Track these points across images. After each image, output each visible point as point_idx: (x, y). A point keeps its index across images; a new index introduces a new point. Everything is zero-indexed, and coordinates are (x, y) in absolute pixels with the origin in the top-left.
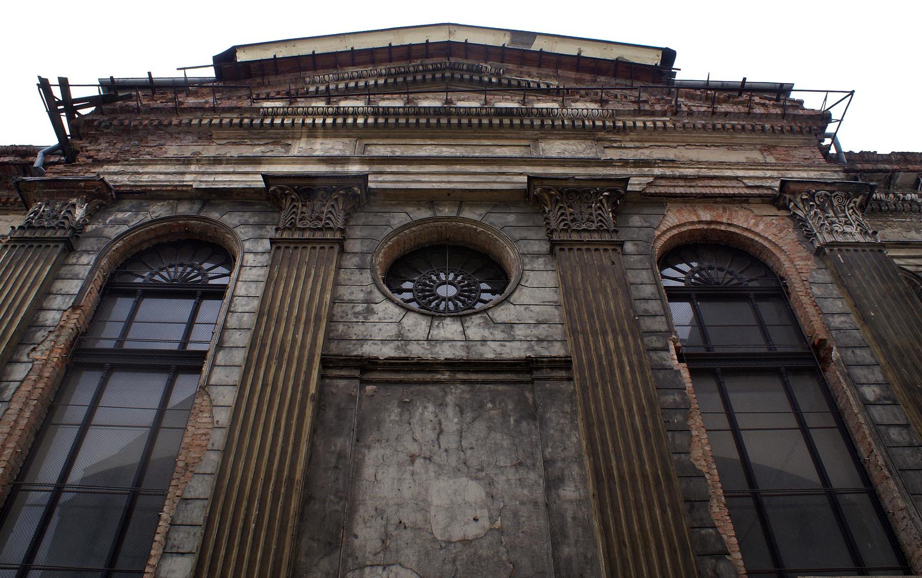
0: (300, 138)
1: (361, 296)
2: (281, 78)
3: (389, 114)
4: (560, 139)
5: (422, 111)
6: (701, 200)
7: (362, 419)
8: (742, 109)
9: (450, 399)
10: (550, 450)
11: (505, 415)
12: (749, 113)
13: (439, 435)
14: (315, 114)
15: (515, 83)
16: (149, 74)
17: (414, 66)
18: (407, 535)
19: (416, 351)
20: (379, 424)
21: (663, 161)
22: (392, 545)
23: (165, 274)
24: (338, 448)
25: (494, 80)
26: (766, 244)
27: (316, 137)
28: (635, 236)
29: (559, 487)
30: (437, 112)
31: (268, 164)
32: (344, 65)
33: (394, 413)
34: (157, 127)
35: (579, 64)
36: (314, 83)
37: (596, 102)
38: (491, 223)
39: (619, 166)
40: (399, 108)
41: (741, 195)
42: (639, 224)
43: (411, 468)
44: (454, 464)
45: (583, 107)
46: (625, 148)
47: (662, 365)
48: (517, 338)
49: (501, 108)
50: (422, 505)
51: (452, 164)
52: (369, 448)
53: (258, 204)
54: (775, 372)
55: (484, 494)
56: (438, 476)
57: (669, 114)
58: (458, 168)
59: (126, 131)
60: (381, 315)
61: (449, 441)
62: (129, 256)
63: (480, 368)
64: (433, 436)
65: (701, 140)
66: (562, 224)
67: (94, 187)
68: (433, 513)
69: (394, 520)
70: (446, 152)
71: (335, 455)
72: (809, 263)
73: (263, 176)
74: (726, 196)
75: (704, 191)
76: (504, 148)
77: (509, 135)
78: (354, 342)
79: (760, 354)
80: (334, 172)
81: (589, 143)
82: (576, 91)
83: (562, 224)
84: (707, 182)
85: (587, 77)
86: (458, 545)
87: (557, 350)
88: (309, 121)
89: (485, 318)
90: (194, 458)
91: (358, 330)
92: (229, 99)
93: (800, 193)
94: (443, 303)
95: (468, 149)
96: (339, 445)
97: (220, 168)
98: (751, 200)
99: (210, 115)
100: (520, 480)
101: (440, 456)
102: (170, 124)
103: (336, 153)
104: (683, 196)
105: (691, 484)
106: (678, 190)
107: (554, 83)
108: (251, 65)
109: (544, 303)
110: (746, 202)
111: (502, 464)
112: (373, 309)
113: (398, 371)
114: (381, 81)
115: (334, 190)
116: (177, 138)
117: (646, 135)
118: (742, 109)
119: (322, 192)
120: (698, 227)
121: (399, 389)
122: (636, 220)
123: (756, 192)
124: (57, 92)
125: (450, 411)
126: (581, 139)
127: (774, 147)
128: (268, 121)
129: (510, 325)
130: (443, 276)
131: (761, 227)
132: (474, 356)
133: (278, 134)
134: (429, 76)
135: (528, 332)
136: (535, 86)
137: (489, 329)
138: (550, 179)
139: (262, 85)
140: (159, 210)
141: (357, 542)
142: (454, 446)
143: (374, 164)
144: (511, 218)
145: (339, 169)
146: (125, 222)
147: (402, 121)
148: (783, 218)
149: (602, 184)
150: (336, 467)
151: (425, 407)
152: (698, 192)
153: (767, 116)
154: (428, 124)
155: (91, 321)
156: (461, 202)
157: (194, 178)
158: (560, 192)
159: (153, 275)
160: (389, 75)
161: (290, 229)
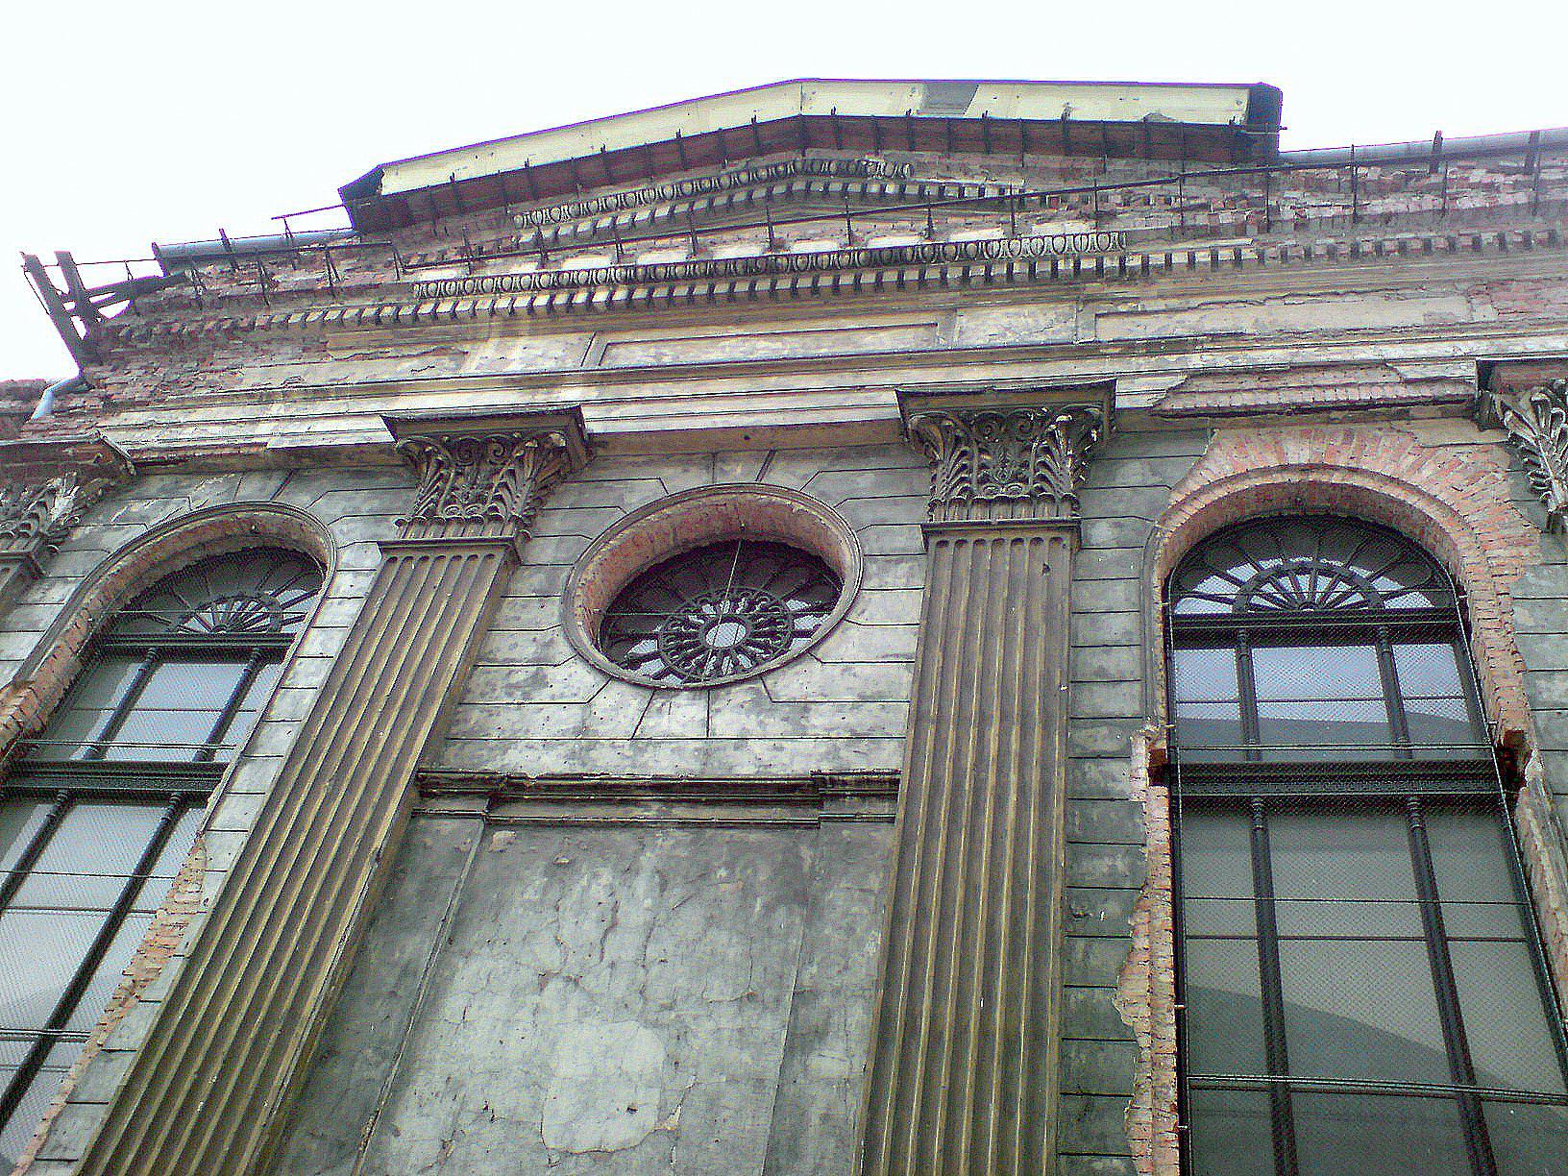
0: (486, 340)
2: (469, 219)
3: (657, 280)
4: (1001, 305)
5: (721, 268)
6: (1294, 418)
7: (468, 897)
8: (1429, 202)
9: (648, 860)
10: (814, 970)
11: (747, 893)
13: (606, 932)
15: (933, 191)
16: (222, 231)
18: (493, 1134)
19: (609, 762)
20: (499, 908)
21: (1215, 337)
22: (457, 1151)
23: (207, 617)
24: (406, 956)
25: (890, 189)
26: (1432, 511)
27: (517, 335)
28: (1121, 508)
29: (812, 1049)
30: (750, 268)
32: (589, 186)
34: (232, 332)
35: (1069, 139)
36: (531, 225)
38: (822, 494)
39: (1112, 355)
40: (676, 265)
41: (1388, 404)
43: (536, 999)
44: (619, 995)
45: (1060, 231)
46: (1145, 313)
47: (1106, 791)
48: (811, 732)
49: (880, 250)
50: (536, 1077)
51: (762, 375)
52: (467, 955)
53: (385, 474)
54: (1394, 806)
55: (661, 1057)
56: (584, 1014)
57: (1252, 230)
58: (772, 382)
59: (177, 344)
60: (557, 688)
61: (624, 946)
64: (595, 935)
65: (1323, 281)
66: (959, 488)
67: (90, 456)
68: (552, 1093)
69: (476, 1103)
70: (764, 349)
71: (398, 970)
72: (1526, 552)
73: (386, 419)
74: (1352, 406)
76: (882, 334)
79: (1380, 765)
81: (1064, 308)
82: (1060, 197)
83: (959, 488)
84: (1309, 378)
85: (1088, 163)
86: (585, 1160)
87: (887, 758)
88: (503, 303)
89: (758, 691)
90: (149, 971)
91: (507, 720)
92: (369, 268)
93: (1528, 387)
95: (808, 340)
96: (410, 949)
97: (322, 407)
98: (1413, 411)
99: (325, 302)
100: (740, 1031)
101: (597, 977)
102: (252, 326)
103: (549, 365)
104: (1248, 412)
105: (1100, 1056)
106: (1239, 401)
107: (1017, 184)
108: (410, 201)
109: (887, 660)
110: (1403, 415)
111: (713, 997)
113: (560, 802)
114: (662, 212)
115: (515, 443)
116: (264, 352)
117: (1194, 281)
118: (1429, 202)
119: (494, 446)
120: (1278, 478)
121: (557, 837)
122: (1133, 472)
123: (1426, 392)
124: (58, 280)
125: (642, 884)
127: (1503, 283)
128: (426, 309)
129: (804, 706)
130: (707, 609)
131: (1427, 472)
132: (715, 771)
133: (446, 333)
134: (760, 193)
135: (837, 719)
137: (759, 714)
139: (432, 237)
140: (206, 493)
141: (395, 1144)
142: (629, 955)
144: (865, 482)
145: (541, 397)
146: (143, 519)
147: (681, 291)
148: (1486, 448)
149: (1056, 397)
150: (393, 993)
151: (596, 876)
153: (1492, 212)
154: (731, 296)
155: (56, 709)
156: (772, 452)
157: (275, 431)
159: (187, 618)
160: (681, 197)
161: (421, 522)
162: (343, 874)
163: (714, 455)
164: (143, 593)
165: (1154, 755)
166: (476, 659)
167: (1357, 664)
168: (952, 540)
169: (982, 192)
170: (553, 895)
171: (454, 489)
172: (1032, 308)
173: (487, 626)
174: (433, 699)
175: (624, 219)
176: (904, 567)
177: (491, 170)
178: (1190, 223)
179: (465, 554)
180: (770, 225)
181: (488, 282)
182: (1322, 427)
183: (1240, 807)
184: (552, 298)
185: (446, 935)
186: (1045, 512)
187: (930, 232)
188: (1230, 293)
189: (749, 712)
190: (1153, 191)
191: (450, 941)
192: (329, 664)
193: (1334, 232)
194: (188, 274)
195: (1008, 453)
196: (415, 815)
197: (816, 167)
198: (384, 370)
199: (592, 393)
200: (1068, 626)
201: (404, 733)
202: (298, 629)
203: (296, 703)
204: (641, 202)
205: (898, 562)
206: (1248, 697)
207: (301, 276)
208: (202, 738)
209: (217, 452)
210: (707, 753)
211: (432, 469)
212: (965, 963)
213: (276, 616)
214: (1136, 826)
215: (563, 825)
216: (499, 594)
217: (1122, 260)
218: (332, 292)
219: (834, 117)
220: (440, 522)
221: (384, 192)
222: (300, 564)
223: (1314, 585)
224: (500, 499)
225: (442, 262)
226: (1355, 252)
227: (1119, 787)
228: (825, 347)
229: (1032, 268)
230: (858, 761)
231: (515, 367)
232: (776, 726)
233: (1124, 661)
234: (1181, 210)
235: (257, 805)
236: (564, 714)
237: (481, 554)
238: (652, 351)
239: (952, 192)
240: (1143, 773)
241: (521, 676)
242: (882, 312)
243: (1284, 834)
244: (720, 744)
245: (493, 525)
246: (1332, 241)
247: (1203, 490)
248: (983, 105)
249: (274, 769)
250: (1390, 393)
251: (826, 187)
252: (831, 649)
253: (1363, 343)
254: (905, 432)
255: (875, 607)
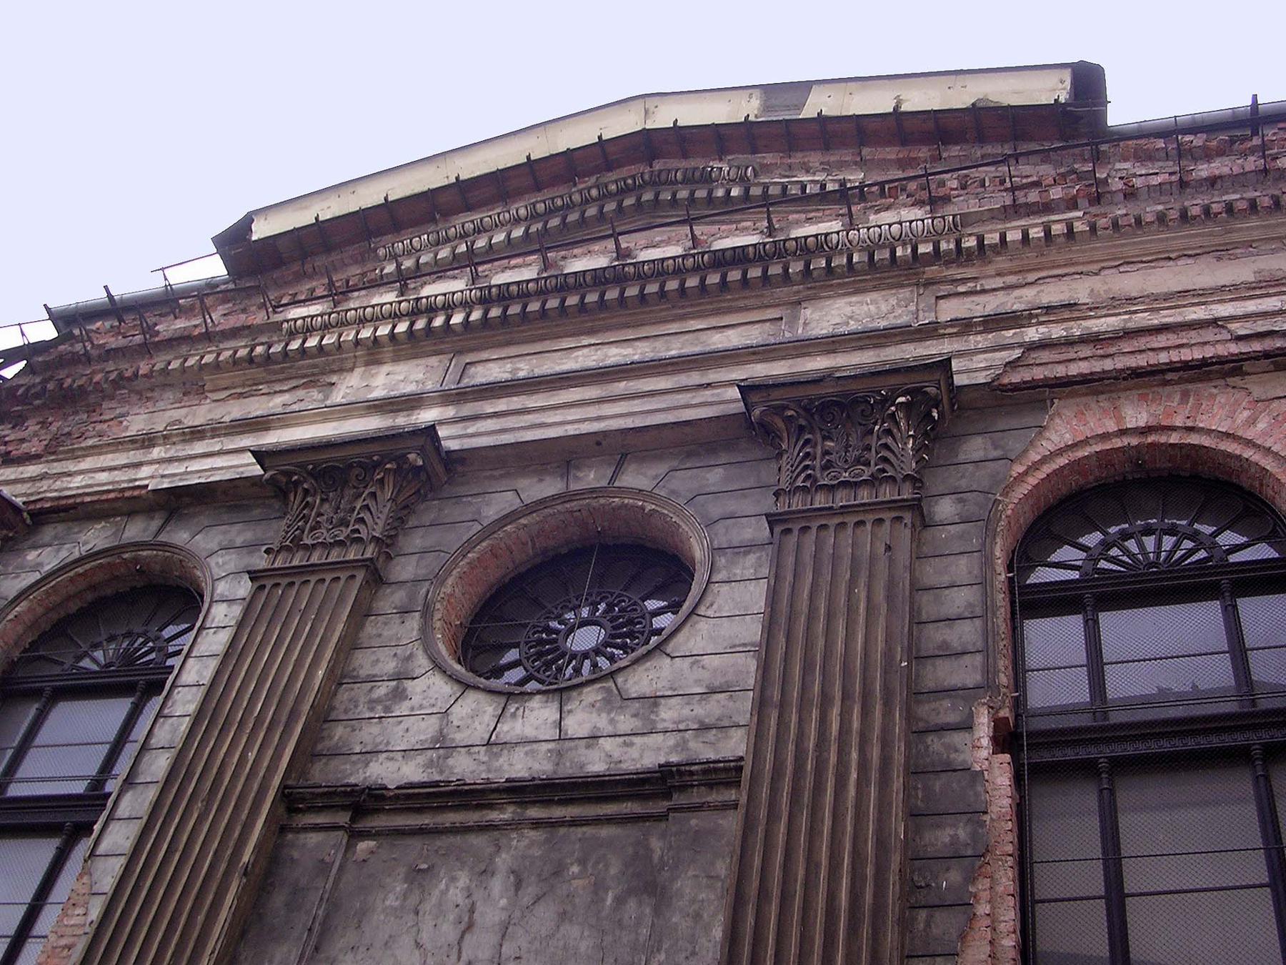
0: (352, 370)
1: (390, 666)
2: (335, 257)
4: (844, 295)
5: (571, 280)
6: (1131, 382)
7: (333, 905)
8: (1252, 163)
9: (504, 861)
10: (662, 957)
11: (598, 888)
12: (1265, 171)
14: (376, 319)
17: (580, 192)
19: (464, 768)
20: (363, 913)
21: (1049, 309)
23: (99, 654)
25: (735, 192)
27: (379, 362)
28: (963, 484)
30: (598, 278)
31: (281, 427)
32: (448, 213)
33: (394, 892)
34: (117, 384)
35: (900, 128)
37: (919, 203)
38: (673, 492)
40: (528, 281)
41: (1221, 361)
42: (978, 455)
46: (984, 291)
47: (948, 763)
48: (660, 726)
49: (724, 251)
57: (1083, 202)
58: (621, 387)
62: (45, 626)
63: (576, 794)
70: (615, 355)
74: (1186, 366)
75: (1132, 362)
77: (741, 303)
78: (354, 758)
80: (393, 428)
81: (905, 293)
84: (1142, 343)
85: (923, 152)
87: (735, 745)
89: (608, 690)
91: (369, 734)
92: (244, 311)
94: (587, 663)
95: (659, 344)
97: (199, 447)
98: (1247, 366)
102: (136, 375)
103: (410, 388)
104: (1086, 381)
106: (1074, 369)
107: (855, 177)
109: (733, 650)
112: (405, 690)
113: (419, 811)
115: (376, 465)
116: (148, 399)
117: (1030, 256)
120: (1117, 443)
121: (416, 843)
122: (975, 448)
123: (1257, 346)
125: (497, 884)
126: (891, 287)
129: (654, 700)
131: (1261, 425)
132: (568, 770)
133: (315, 366)
136: (816, 189)
138: (783, 385)
139: (301, 276)
140: (95, 537)
143: (466, 401)
144: (714, 477)
146: (36, 567)
149: (894, 380)
151: (453, 879)
152: (1119, 366)
156: (624, 456)
157: (155, 473)
158: (805, 409)
159: (80, 658)
160: (533, 217)
161: (288, 549)
162: (214, 889)
163: (568, 462)
164: (40, 636)
165: (998, 724)
166: (339, 676)
167: (1198, 622)
168: (796, 527)
169: (823, 186)
170: (413, 900)
171: (321, 515)
172: (874, 295)
173: (350, 645)
174: (299, 717)
175: (481, 243)
176: (752, 558)
177: (353, 208)
178: (1022, 200)
179: (329, 577)
180: (615, 236)
181: (351, 314)
182: (1160, 390)
183: (1087, 769)
184: (412, 324)
185: (312, 943)
186: (887, 493)
187: (771, 230)
188: (1053, 267)
189: (599, 711)
190: (987, 173)
191: (317, 949)
192: (203, 690)
193: (1163, 199)
194: (76, 332)
195: (851, 436)
196: (283, 829)
197: (663, 177)
198: (256, 407)
199: (450, 412)
200: (912, 606)
201: (270, 752)
202: (176, 662)
203: (175, 730)
204: (497, 226)
205: (746, 553)
206: (1238, 650)
207: (180, 324)
208: (93, 770)
209: (104, 497)
210: (560, 753)
211: (299, 498)
212: (805, 939)
213: (161, 649)
214: (977, 795)
215: (421, 831)
216: (362, 613)
217: (958, 243)
218: (208, 337)
219: (676, 129)
220: (306, 547)
221: (254, 238)
222: (181, 598)
223: (1159, 544)
224: (362, 520)
225: (311, 299)
226: (1184, 216)
227: (961, 758)
228: (675, 349)
229: (871, 256)
230: (704, 750)
231: (378, 393)
232: (626, 723)
233: (967, 633)
234: (1013, 189)
235: (134, 829)
236: (423, 725)
237: (343, 576)
238: (509, 367)
239: (794, 190)
240: (985, 742)
241: (382, 690)
242: (730, 311)
243: (1129, 794)
244: (572, 744)
245: (355, 547)
246: (1160, 208)
247: (1044, 460)
248: (818, 105)
249: (152, 793)
250: (1222, 350)
251: (674, 195)
252: (683, 643)
253: (1193, 305)
254: (751, 425)
255: (724, 599)
